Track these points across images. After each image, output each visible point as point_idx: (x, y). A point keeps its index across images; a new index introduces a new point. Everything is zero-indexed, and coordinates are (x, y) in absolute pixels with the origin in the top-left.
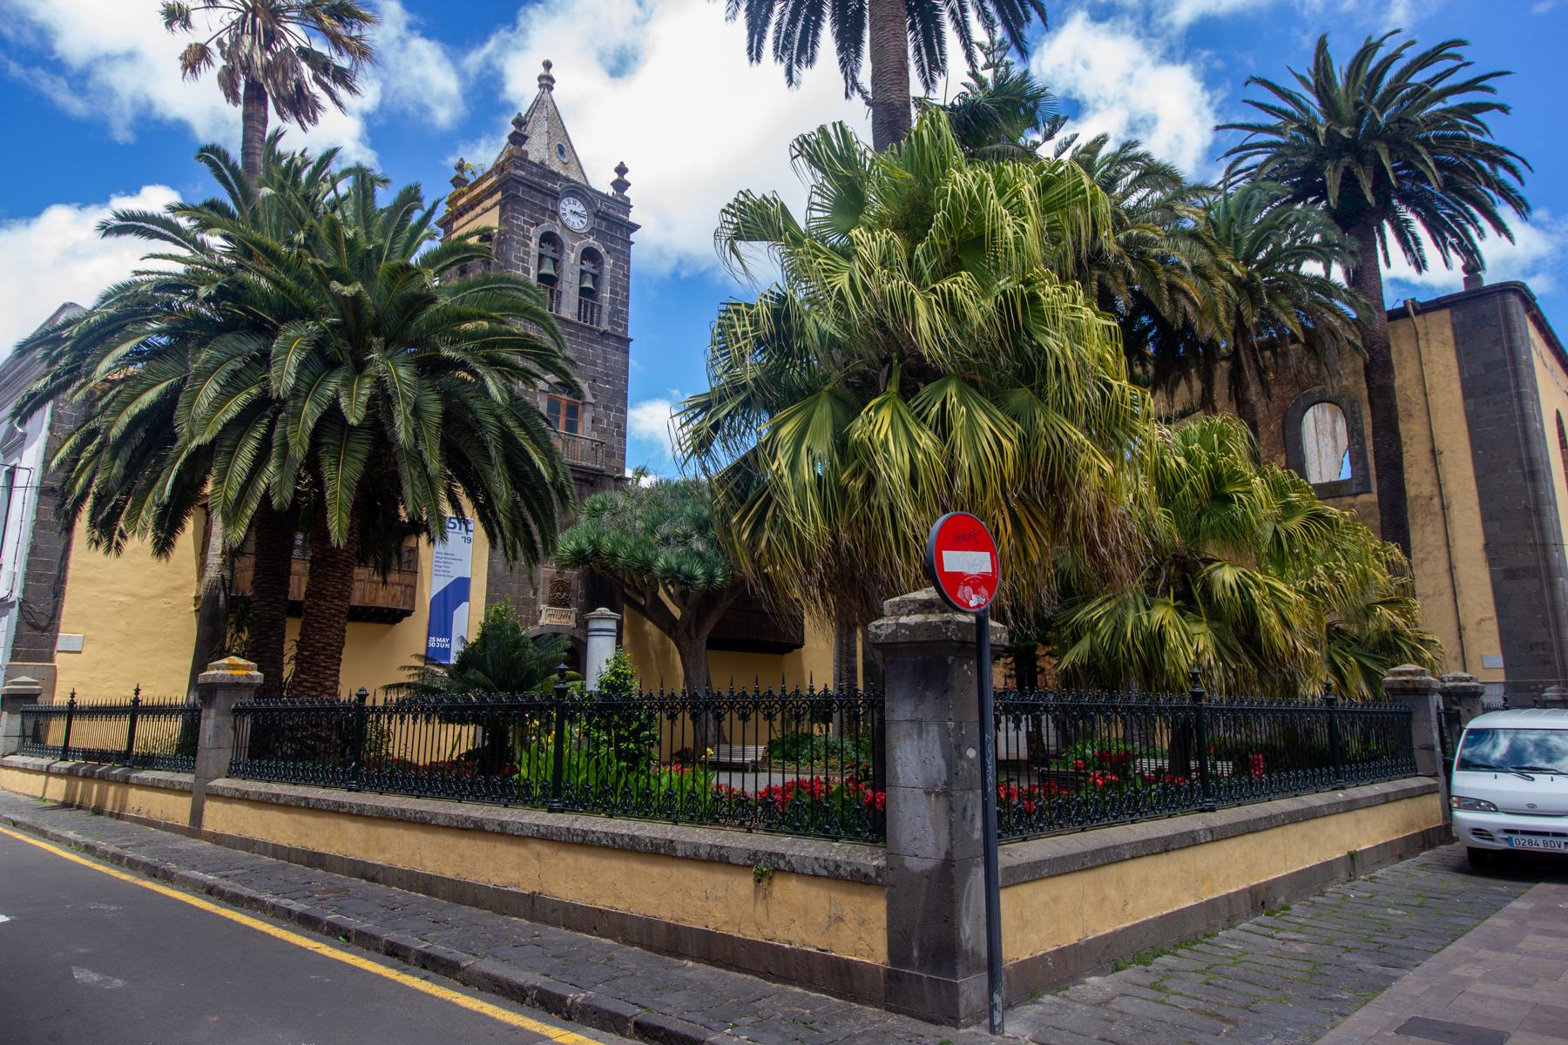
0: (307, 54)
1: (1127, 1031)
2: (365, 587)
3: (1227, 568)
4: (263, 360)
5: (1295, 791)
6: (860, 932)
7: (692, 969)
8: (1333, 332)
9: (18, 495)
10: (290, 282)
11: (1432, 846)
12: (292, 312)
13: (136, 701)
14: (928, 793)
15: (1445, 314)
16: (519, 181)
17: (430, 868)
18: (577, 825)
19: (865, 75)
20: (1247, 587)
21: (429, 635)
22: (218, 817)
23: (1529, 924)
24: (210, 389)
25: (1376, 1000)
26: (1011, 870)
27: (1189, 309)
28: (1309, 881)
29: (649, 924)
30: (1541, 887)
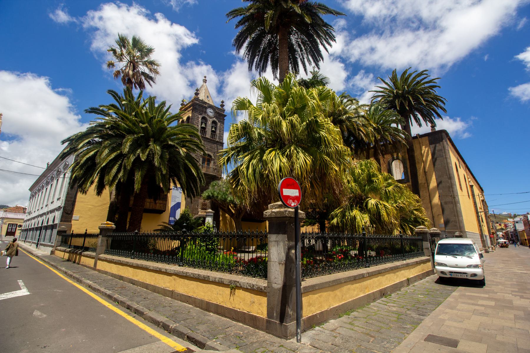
0: (143, 74)
1: (341, 341)
2: (149, 203)
3: (373, 199)
4: (120, 145)
5: (392, 261)
6: (259, 307)
7: (212, 316)
8: (400, 142)
9: (66, 179)
10: (130, 125)
11: (429, 275)
12: (130, 132)
13: (86, 233)
14: (280, 264)
15: (427, 138)
16: (197, 104)
17: (148, 282)
18: (185, 271)
19: (278, 76)
20: (378, 204)
21: (170, 217)
22: (101, 265)
23: (459, 300)
24: (106, 151)
25: (417, 328)
26: (305, 288)
27: (362, 135)
28: (396, 287)
29: (202, 301)
30: (460, 288)
